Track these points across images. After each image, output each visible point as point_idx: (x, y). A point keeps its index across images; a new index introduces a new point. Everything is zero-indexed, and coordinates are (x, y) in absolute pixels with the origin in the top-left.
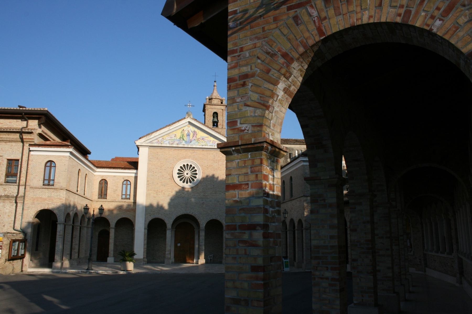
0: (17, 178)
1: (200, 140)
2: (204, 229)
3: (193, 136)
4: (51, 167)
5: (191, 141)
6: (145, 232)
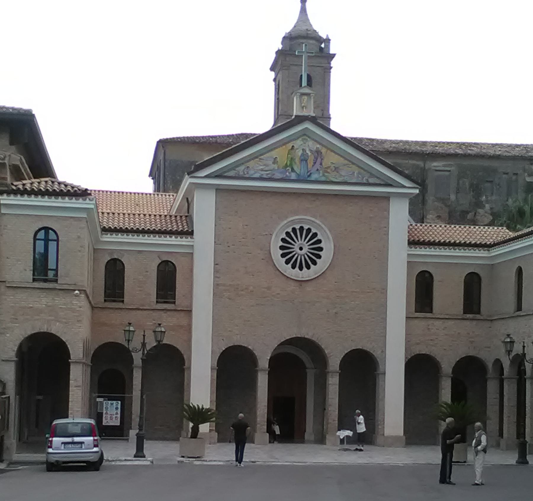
0: (37, 276)
1: (329, 171)
3: (315, 163)
4: (47, 240)
5: (309, 174)
6: (212, 376)
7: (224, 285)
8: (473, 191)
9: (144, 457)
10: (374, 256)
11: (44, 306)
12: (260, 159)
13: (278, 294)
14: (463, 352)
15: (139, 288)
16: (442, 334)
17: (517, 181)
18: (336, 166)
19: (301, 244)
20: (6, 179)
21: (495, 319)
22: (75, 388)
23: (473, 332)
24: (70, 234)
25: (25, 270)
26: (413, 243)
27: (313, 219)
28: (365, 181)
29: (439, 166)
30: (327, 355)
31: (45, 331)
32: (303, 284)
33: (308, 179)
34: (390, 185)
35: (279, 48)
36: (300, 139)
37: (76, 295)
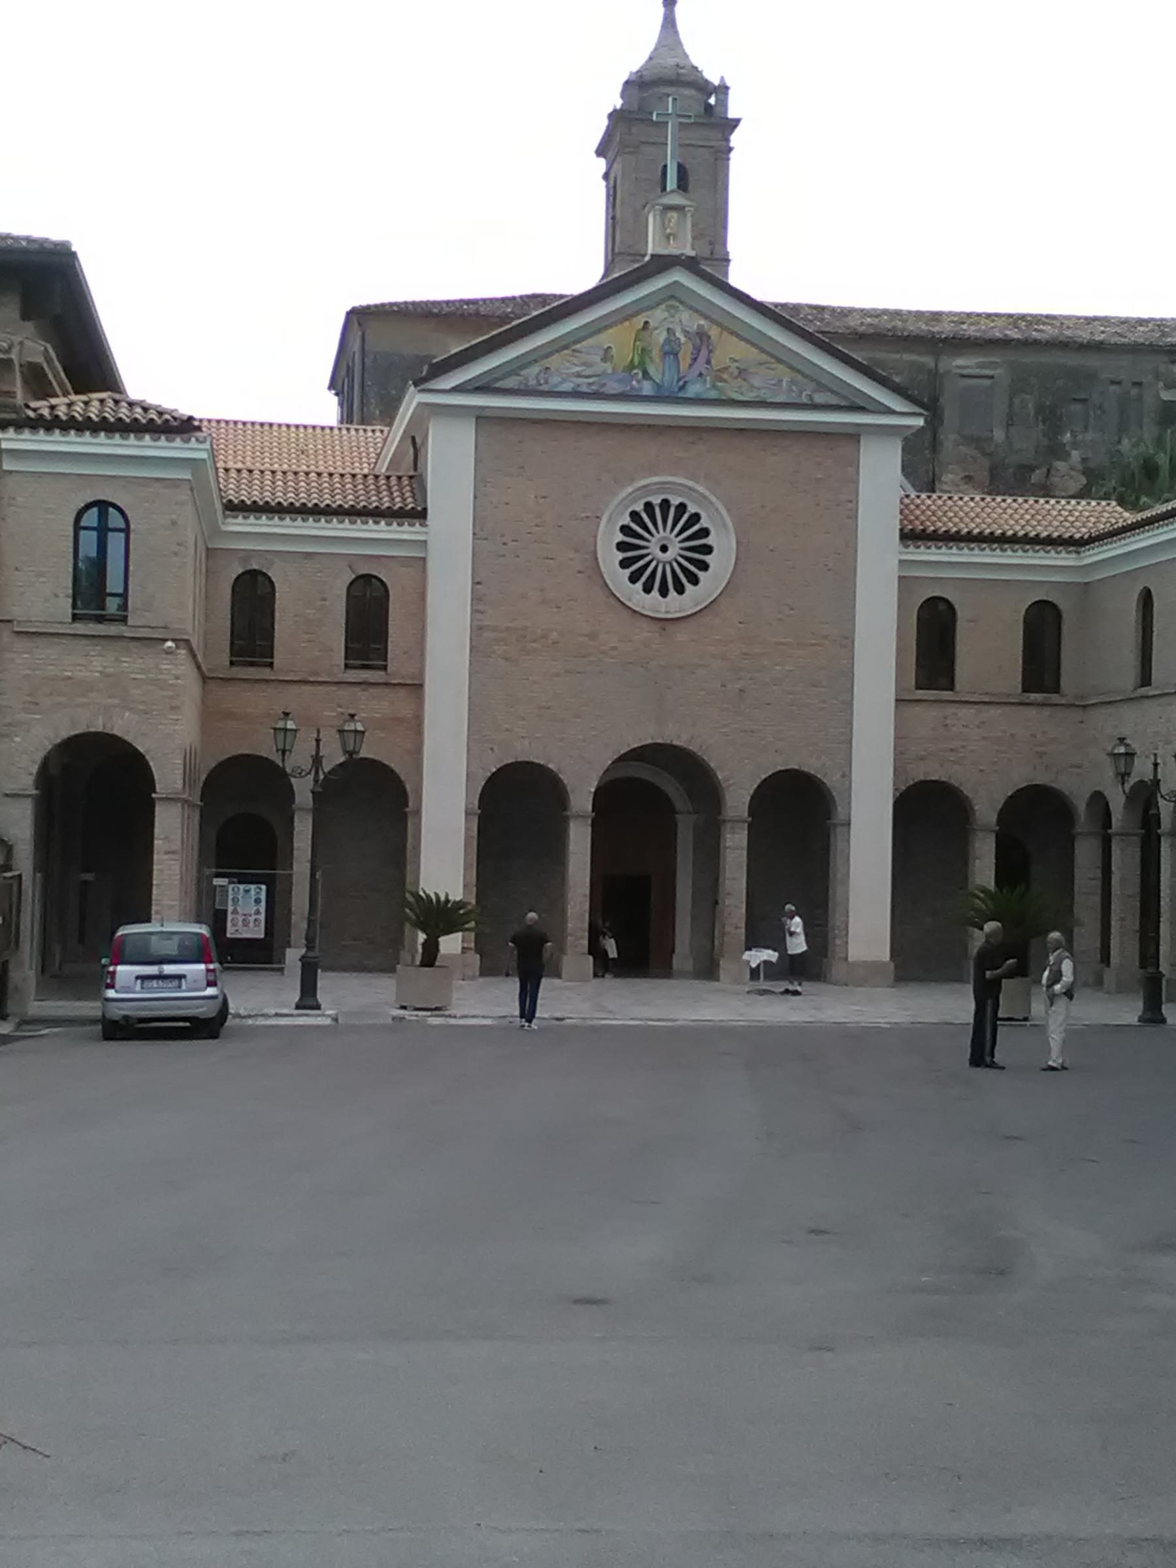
0: (82, 609)
2: (746, 814)
3: (695, 360)
5: (681, 383)
6: (467, 829)
7: (494, 629)
8: (1044, 422)
9: (318, 1007)
10: (826, 565)
11: (97, 674)
12: (574, 350)
13: (614, 648)
14: (1021, 776)
15: (306, 636)
16: (976, 738)
17: (1140, 398)
18: (743, 367)
19: (665, 538)
20: (13, 395)
21: (1092, 705)
22: (166, 857)
23: (1044, 733)
24: (154, 516)
25: (56, 596)
26: (911, 536)
27: (691, 483)
28: (805, 400)
29: (968, 367)
30: (722, 782)
31: (100, 729)
32: (670, 627)
33: (680, 395)
34: (861, 409)
35: (615, 106)
36: (663, 307)
37: (169, 652)
